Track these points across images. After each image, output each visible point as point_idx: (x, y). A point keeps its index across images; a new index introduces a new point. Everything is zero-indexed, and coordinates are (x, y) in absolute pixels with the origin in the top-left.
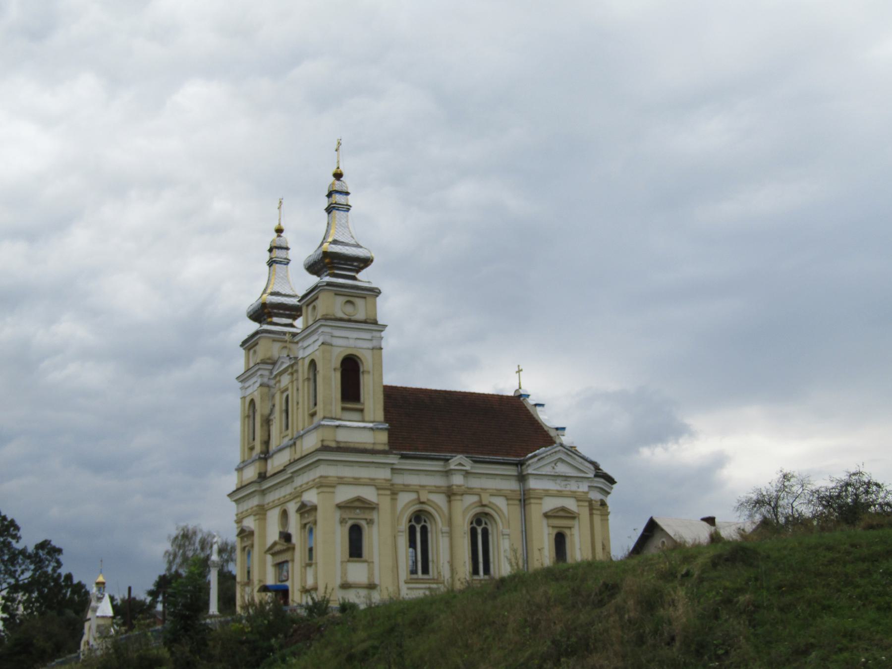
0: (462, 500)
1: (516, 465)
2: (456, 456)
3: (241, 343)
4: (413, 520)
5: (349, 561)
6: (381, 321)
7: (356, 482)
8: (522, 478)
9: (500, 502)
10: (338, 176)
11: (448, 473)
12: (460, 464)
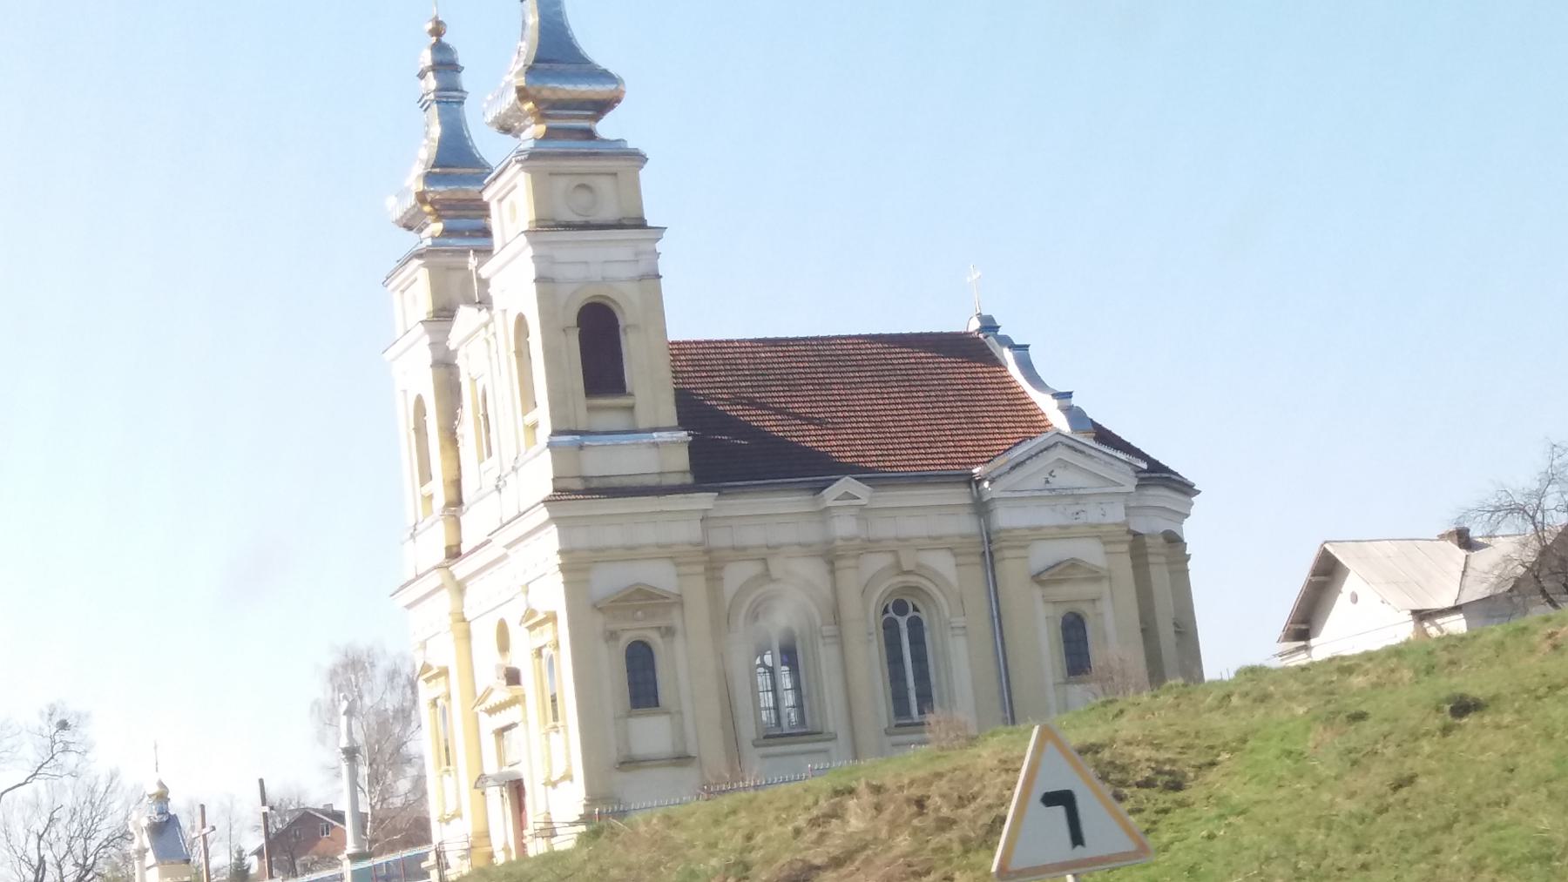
2: (837, 480)
7: (631, 553)
9: (942, 563)
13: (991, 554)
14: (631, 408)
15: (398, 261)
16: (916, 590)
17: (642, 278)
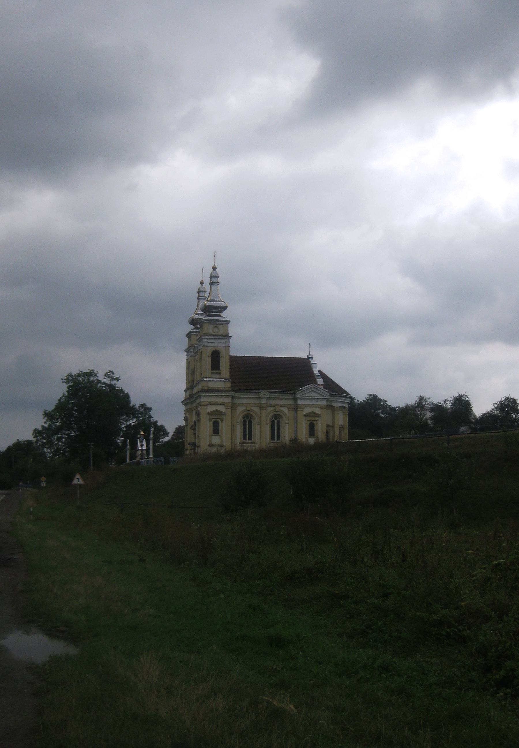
0: (265, 410)
1: (292, 394)
3: (186, 335)
4: (245, 418)
5: (213, 435)
6: (230, 335)
8: (295, 399)
9: (285, 410)
10: (214, 268)
11: (260, 398)
12: (265, 395)
13: (296, 409)
14: (220, 373)
15: (317, 402)
16: (279, 415)
17: (226, 347)
